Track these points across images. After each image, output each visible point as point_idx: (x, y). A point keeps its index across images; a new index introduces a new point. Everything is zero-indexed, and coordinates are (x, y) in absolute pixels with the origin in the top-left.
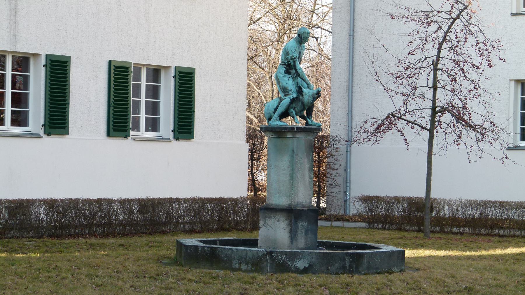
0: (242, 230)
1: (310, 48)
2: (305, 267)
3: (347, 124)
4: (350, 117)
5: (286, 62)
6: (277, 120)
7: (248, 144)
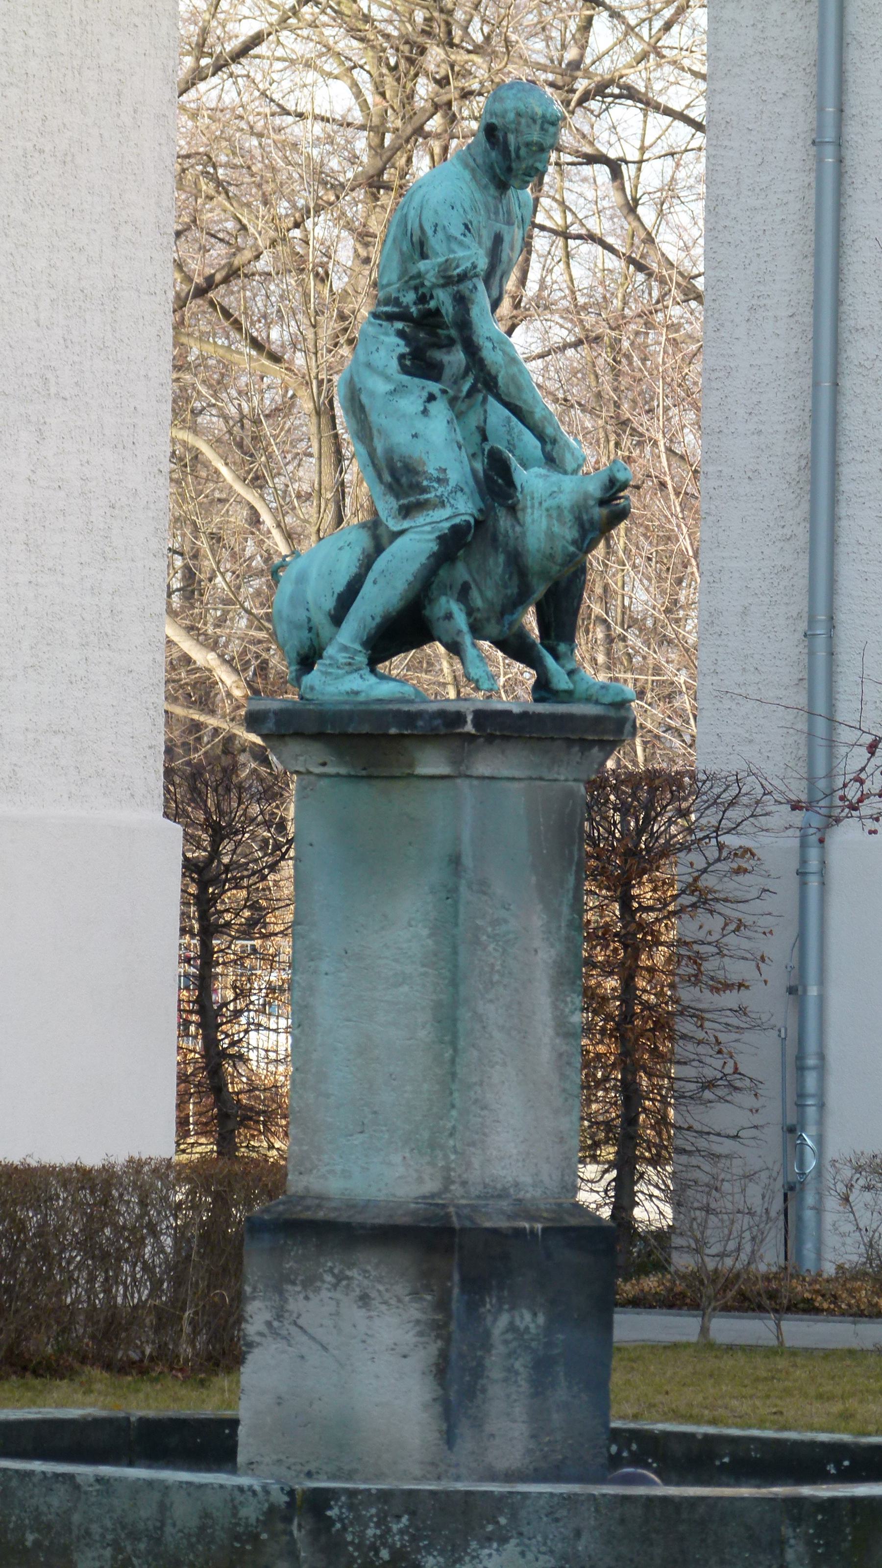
0: (140, 1369)
1: (575, 229)
3: (802, 700)
4: (821, 654)
5: (409, 298)
6: (352, 668)
7: (176, 830)
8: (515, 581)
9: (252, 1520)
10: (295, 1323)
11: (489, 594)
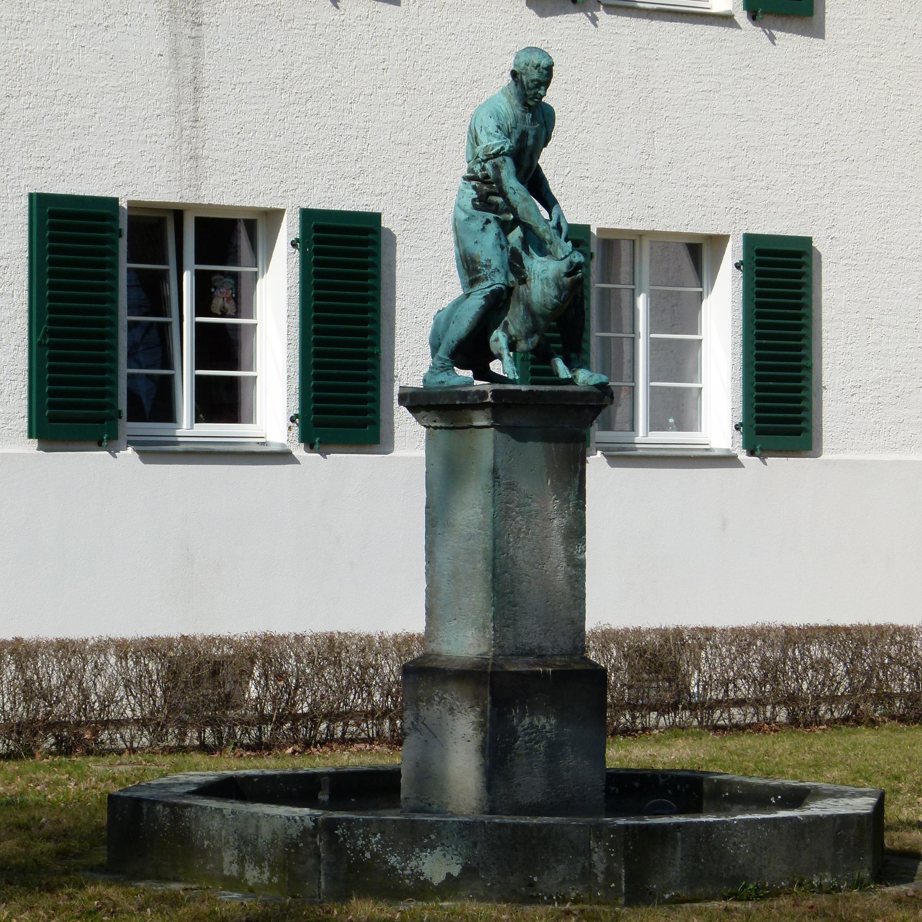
2: (449, 875)
8: (530, 319)
9: (295, 836)
10: (423, 723)
11: (518, 327)
